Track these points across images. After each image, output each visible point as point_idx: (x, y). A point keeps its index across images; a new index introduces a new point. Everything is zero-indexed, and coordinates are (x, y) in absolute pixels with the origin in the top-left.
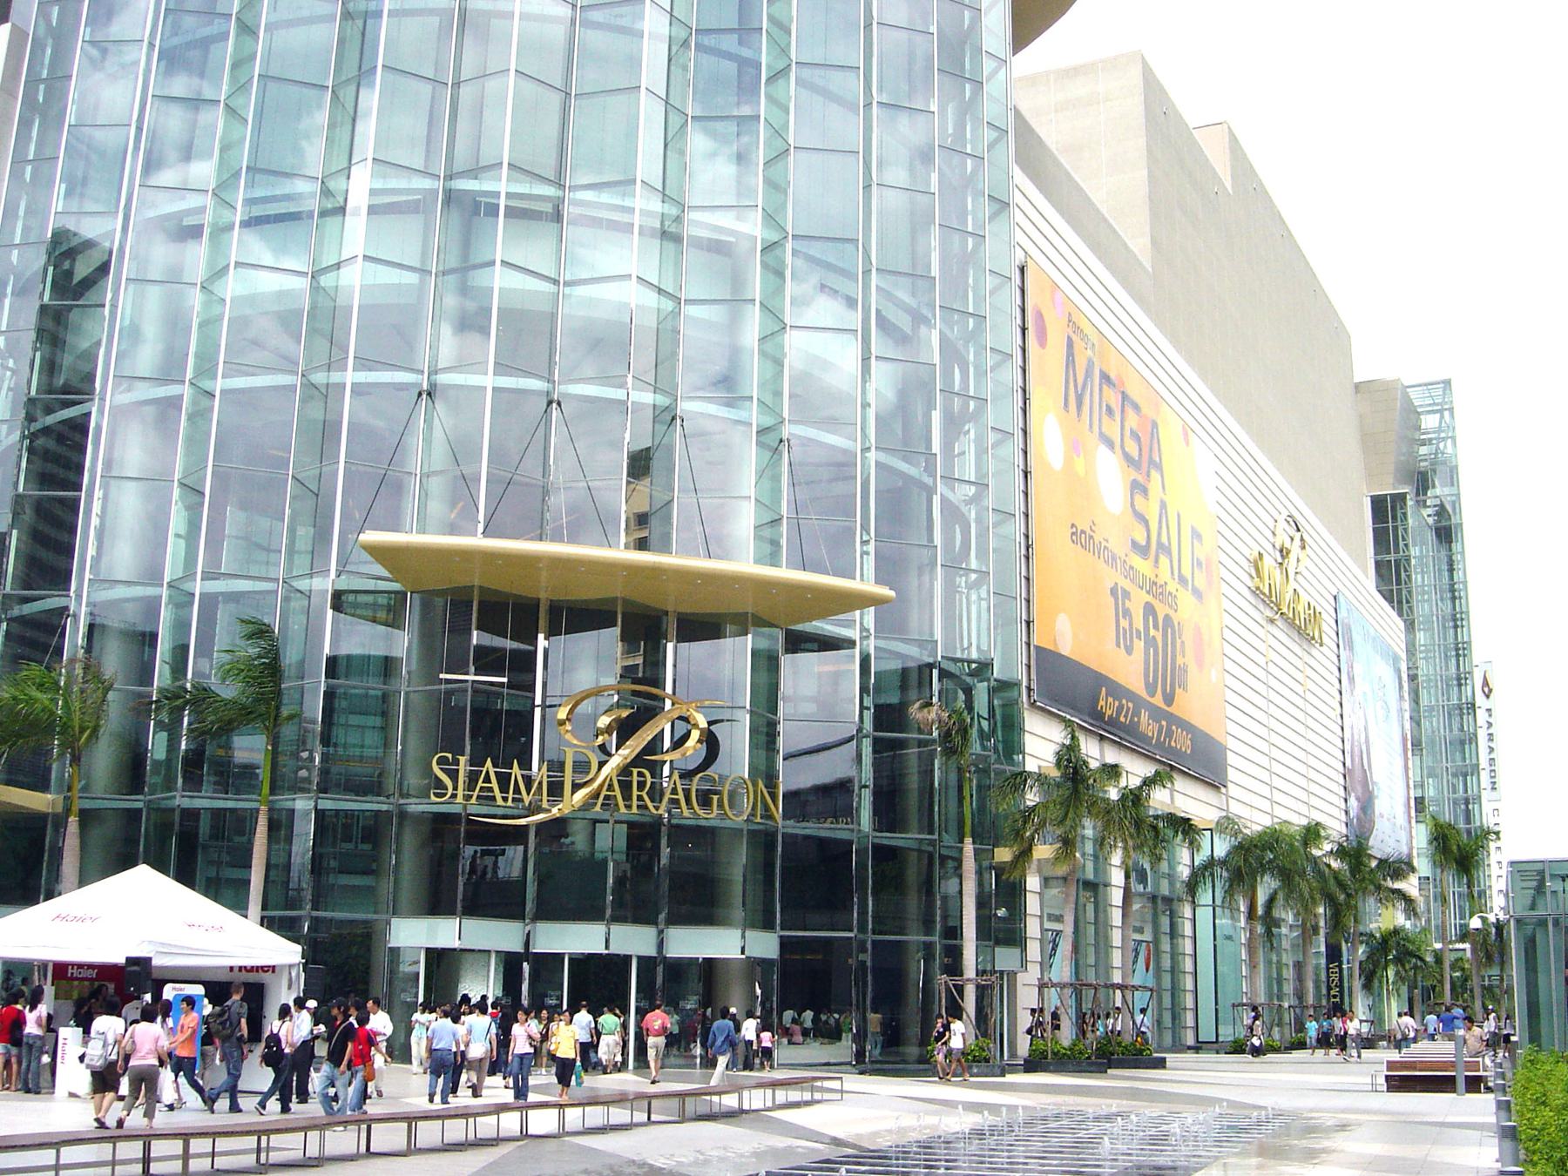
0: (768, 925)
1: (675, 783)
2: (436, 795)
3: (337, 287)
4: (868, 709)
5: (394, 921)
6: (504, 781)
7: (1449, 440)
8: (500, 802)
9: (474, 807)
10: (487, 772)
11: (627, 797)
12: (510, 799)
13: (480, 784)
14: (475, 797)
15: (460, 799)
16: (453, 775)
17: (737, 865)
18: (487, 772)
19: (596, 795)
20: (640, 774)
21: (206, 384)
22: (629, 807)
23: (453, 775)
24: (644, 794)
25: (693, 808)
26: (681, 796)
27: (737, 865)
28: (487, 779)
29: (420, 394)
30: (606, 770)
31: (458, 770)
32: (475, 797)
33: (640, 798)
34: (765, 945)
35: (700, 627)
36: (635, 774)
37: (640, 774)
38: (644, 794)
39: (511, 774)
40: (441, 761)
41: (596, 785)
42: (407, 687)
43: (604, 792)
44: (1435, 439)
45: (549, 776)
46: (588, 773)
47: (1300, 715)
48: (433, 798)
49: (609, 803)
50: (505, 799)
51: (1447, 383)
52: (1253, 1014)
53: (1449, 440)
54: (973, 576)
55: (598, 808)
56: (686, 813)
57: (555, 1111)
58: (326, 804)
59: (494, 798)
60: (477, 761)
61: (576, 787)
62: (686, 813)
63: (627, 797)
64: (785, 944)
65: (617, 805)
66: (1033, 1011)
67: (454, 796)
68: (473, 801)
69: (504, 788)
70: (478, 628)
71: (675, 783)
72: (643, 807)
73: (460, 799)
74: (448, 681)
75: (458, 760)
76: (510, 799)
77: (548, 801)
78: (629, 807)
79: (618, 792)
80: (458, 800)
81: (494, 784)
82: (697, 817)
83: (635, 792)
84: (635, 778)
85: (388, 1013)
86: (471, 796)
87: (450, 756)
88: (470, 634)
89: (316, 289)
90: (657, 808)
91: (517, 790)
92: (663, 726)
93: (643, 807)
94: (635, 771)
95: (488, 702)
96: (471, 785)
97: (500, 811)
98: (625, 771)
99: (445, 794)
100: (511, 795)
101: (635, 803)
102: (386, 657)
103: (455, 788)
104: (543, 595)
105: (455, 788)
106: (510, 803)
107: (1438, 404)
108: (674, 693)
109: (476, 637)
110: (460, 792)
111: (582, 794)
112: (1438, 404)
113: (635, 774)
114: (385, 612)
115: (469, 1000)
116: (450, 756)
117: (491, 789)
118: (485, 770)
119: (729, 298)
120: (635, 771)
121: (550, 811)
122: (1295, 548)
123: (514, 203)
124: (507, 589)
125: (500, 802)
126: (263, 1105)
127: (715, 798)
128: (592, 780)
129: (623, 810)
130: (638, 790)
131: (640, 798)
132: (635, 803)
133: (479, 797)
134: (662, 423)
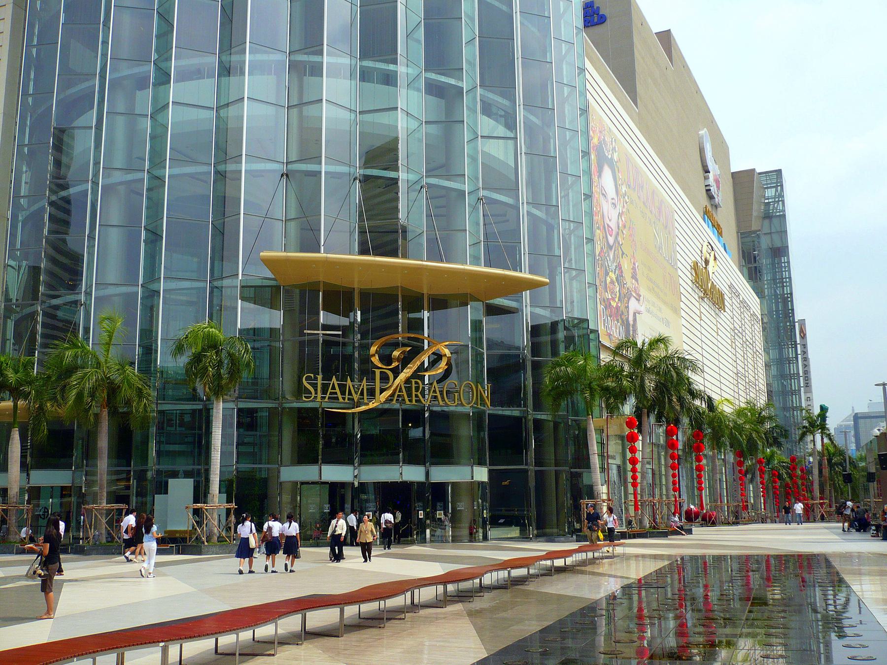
0: (481, 463)
1: (435, 387)
3: (228, 117)
5: (282, 469)
6: (342, 388)
7: (781, 202)
8: (341, 400)
9: (327, 405)
10: (333, 384)
11: (410, 395)
12: (347, 399)
13: (330, 390)
14: (327, 398)
15: (319, 399)
16: (315, 386)
17: (465, 432)
18: (333, 384)
19: (392, 395)
20: (416, 383)
21: (157, 173)
22: (410, 401)
23: (315, 386)
24: (419, 393)
25: (445, 401)
26: (438, 394)
27: (465, 432)
28: (334, 388)
29: (282, 175)
30: (398, 381)
31: (317, 383)
32: (327, 398)
33: (416, 396)
34: (482, 474)
35: (439, 303)
36: (413, 383)
37: (416, 383)
38: (419, 393)
39: (346, 385)
40: (308, 378)
42: (287, 347)
43: (397, 393)
44: (772, 202)
45: (367, 385)
46: (388, 383)
48: (304, 399)
50: (344, 399)
53: (781, 202)
54: (574, 273)
56: (441, 403)
57: (769, 236)
58: (242, 405)
59: (337, 398)
61: (382, 391)
62: (441, 403)
64: (490, 471)
65: (404, 400)
67: (316, 397)
68: (326, 400)
69: (343, 393)
70: (323, 310)
71: (435, 387)
72: (418, 401)
73: (319, 399)
74: (309, 334)
75: (317, 378)
76: (347, 399)
77: (367, 399)
78: (410, 401)
80: (316, 400)
81: (338, 390)
82: (447, 405)
83: (414, 393)
84: (414, 385)
86: (325, 397)
87: (312, 375)
88: (318, 314)
89: (218, 117)
91: (350, 394)
92: (425, 358)
93: (418, 401)
94: (413, 381)
96: (324, 391)
97: (342, 406)
98: (408, 381)
99: (311, 397)
100: (347, 396)
101: (414, 399)
102: (271, 328)
103: (316, 393)
104: (356, 286)
105: (316, 393)
106: (346, 400)
107: (774, 183)
108: (428, 336)
109: (323, 317)
110: (319, 395)
111: (386, 394)
112: (774, 183)
113: (413, 383)
117: (336, 393)
118: (332, 382)
119: (444, 120)
120: (413, 381)
122: (711, 259)
124: (338, 283)
125: (341, 400)
128: (391, 386)
129: (408, 402)
131: (416, 396)
132: (414, 399)
133: (329, 398)
134: (415, 191)
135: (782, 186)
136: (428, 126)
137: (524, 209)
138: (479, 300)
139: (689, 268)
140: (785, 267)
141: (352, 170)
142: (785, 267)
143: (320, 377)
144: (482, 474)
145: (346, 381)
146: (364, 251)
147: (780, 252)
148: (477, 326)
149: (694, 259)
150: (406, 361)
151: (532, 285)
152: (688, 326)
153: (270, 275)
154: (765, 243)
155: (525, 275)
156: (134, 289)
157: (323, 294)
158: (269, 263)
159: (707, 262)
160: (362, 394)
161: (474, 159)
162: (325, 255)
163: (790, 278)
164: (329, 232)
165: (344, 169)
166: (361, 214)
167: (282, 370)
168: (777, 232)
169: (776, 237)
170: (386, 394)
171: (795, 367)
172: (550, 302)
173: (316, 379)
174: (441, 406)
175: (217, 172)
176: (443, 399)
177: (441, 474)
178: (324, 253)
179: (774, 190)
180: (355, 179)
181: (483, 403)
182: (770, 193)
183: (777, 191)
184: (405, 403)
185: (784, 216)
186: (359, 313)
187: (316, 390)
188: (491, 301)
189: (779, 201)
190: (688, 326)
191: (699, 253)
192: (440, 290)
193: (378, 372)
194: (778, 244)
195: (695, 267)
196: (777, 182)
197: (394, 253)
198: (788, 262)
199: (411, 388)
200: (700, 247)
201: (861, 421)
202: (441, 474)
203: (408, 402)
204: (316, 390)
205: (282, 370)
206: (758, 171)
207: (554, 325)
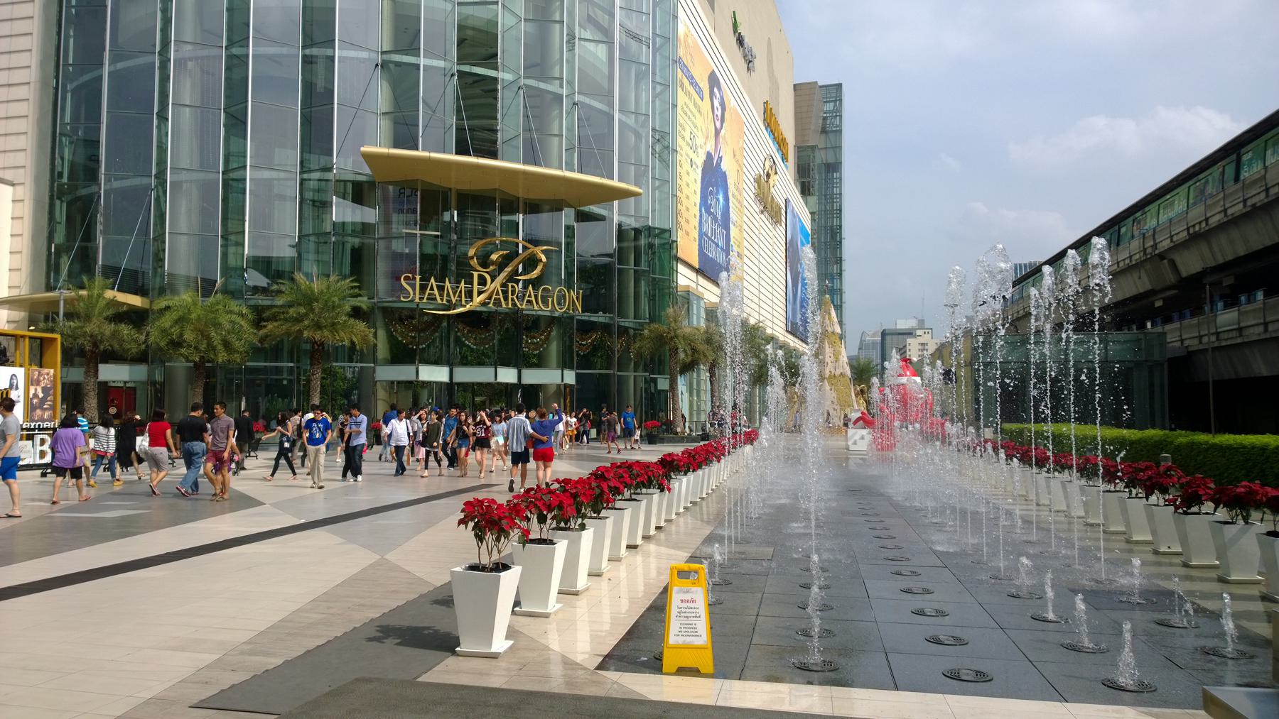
2: (404, 297)
4: (1266, 330)
6: (441, 289)
8: (439, 301)
11: (506, 299)
13: (428, 291)
15: (417, 300)
18: (432, 285)
19: (490, 298)
20: (513, 287)
22: (507, 304)
24: (514, 297)
26: (533, 299)
28: (432, 289)
33: (512, 299)
34: (570, 377)
37: (513, 287)
38: (514, 297)
39: (444, 286)
40: (406, 278)
41: (491, 290)
43: (494, 296)
47: (770, 262)
49: (497, 302)
51: (839, 86)
52: (301, 454)
55: (491, 305)
56: (536, 308)
60: (425, 279)
61: (480, 293)
63: (506, 299)
64: (578, 376)
66: (44, 475)
68: (425, 301)
72: (514, 305)
73: (417, 300)
79: (501, 296)
81: (436, 292)
83: (510, 297)
85: (656, 463)
86: (423, 298)
87: (411, 275)
90: (521, 305)
91: (448, 295)
93: (514, 305)
94: (510, 285)
95: (309, 235)
97: (440, 307)
100: (445, 298)
105: (414, 294)
106: (445, 302)
111: (483, 297)
114: (311, 198)
115: (42, 473)
116: (411, 275)
120: (510, 285)
121: (465, 306)
122: (772, 173)
123: (470, 102)
125: (439, 301)
126: (1137, 494)
127: (550, 299)
128: (487, 290)
130: (512, 295)
131: (512, 299)
133: (428, 299)
135: (841, 100)
136: (528, 24)
137: (617, 116)
138: (571, 206)
139: (752, 181)
140: (837, 183)
141: (448, 65)
142: (837, 183)
143: (418, 277)
144: (570, 377)
145: (445, 282)
146: (462, 150)
147: (833, 167)
148: (569, 229)
149: (757, 172)
150: (501, 266)
151: (623, 194)
152: (749, 239)
153: (367, 171)
154: (820, 157)
155: (615, 183)
156: (212, 176)
157: (421, 195)
158: (369, 158)
159: (768, 175)
160: (460, 296)
161: (571, 62)
162: (426, 154)
163: (840, 194)
164: (425, 127)
165: (441, 64)
166: (459, 111)
167: (1152, 398)
168: (832, 148)
169: (830, 153)
170: (483, 297)
171: (1231, 335)
172: (635, 212)
173: (414, 279)
174: (536, 310)
175: (229, 57)
176: (537, 303)
177: (532, 377)
178: (423, 150)
179: (832, 104)
180: (452, 75)
181: (575, 309)
182: (830, 106)
183: (835, 106)
184: (501, 306)
185: (840, 131)
186: (456, 212)
187: (414, 290)
188: (581, 208)
189: (836, 116)
190: (749, 239)
191: (762, 166)
192: (534, 196)
193: (476, 274)
194: (831, 160)
195: (758, 180)
196: (836, 97)
197: (493, 155)
198: (840, 179)
199: (507, 291)
200: (763, 160)
201: (888, 338)
202: (532, 377)
203: (504, 306)
204: (414, 290)
205: (1152, 398)
206: (820, 83)
207: (637, 232)
